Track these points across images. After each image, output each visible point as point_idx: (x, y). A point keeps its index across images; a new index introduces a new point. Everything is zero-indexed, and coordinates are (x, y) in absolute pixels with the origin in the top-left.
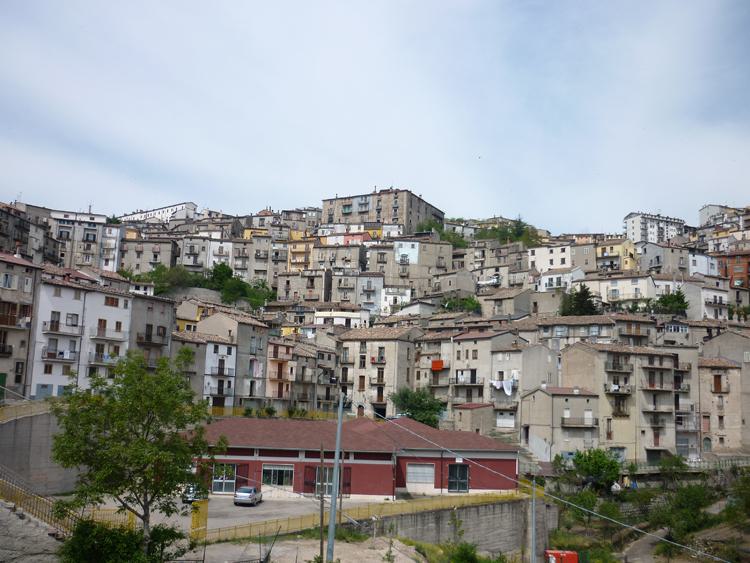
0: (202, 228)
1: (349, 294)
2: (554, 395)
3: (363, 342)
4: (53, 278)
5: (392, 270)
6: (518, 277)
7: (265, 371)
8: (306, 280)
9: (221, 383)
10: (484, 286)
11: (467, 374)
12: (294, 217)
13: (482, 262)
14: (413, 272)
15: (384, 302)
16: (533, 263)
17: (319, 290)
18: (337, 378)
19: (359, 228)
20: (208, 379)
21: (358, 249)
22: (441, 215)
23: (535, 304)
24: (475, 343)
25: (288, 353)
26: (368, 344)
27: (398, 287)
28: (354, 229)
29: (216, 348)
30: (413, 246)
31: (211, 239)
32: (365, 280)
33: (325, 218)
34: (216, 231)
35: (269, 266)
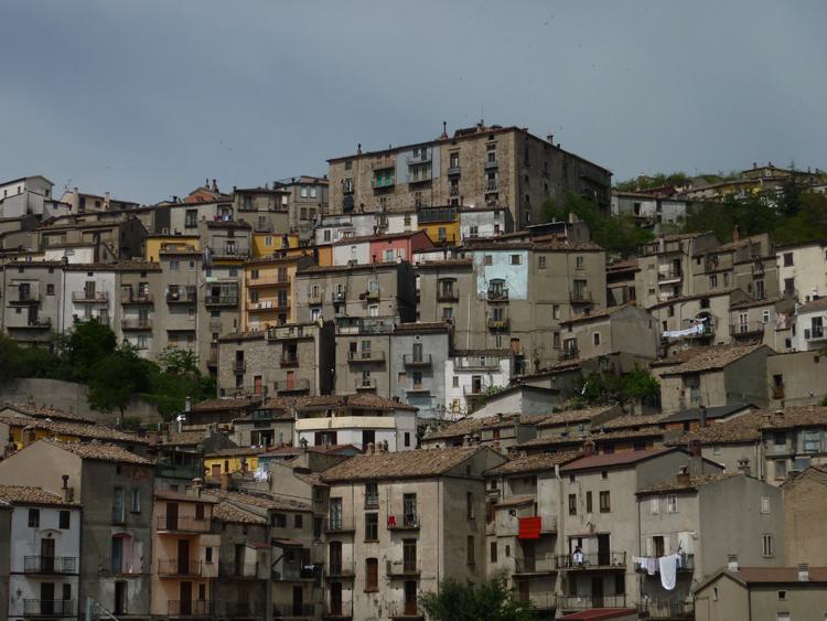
0: (54, 240)
1: (374, 376)
2: (751, 586)
3: (371, 485)
4: (99, 219)
5: (470, 316)
6: (753, 318)
7: (148, 559)
8: (279, 348)
9: (47, 591)
10: (676, 342)
11: (591, 547)
12: (263, 203)
13: (677, 288)
14: (518, 317)
15: (452, 388)
16: (790, 283)
17: (309, 371)
18: (319, 566)
19: (408, 222)
20: (18, 583)
21: (394, 273)
22: (601, 179)
23: (778, 379)
24: (605, 476)
25: (200, 516)
26: (382, 488)
27: (483, 354)
28: (396, 225)
29: (34, 520)
30: (516, 260)
31: (66, 267)
32: (409, 341)
33: (335, 201)
34: (81, 245)
35: (200, 321)
